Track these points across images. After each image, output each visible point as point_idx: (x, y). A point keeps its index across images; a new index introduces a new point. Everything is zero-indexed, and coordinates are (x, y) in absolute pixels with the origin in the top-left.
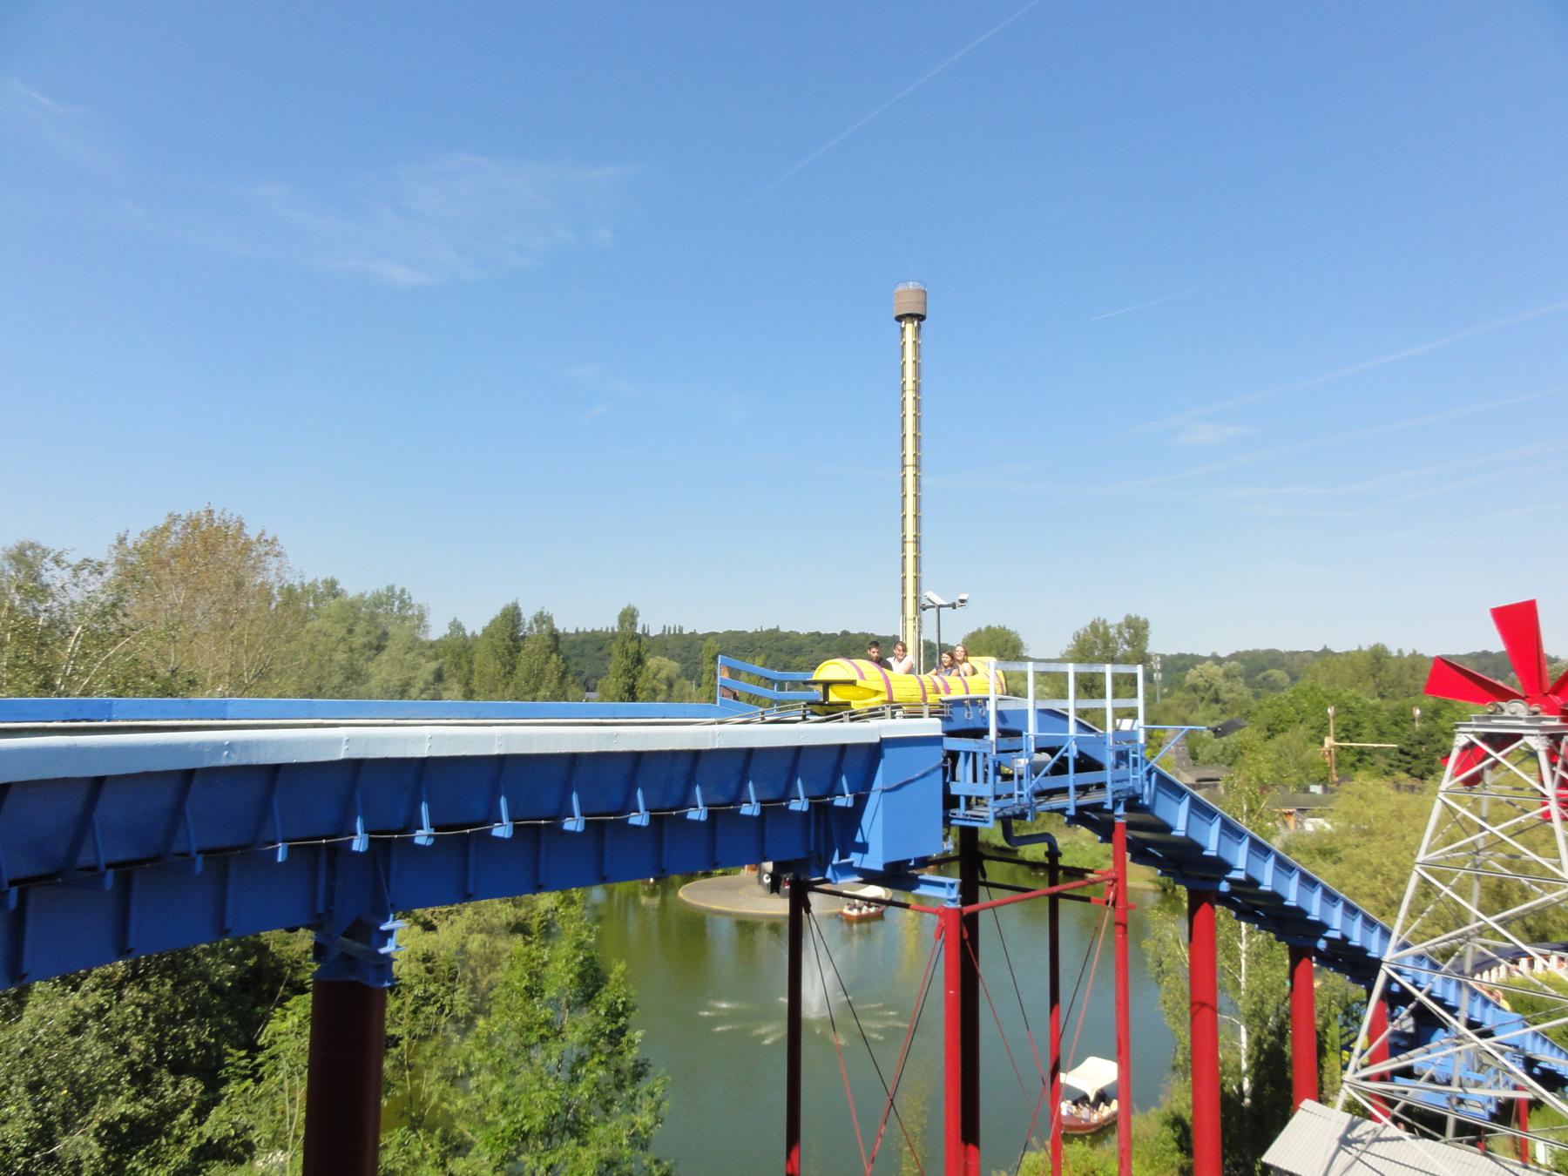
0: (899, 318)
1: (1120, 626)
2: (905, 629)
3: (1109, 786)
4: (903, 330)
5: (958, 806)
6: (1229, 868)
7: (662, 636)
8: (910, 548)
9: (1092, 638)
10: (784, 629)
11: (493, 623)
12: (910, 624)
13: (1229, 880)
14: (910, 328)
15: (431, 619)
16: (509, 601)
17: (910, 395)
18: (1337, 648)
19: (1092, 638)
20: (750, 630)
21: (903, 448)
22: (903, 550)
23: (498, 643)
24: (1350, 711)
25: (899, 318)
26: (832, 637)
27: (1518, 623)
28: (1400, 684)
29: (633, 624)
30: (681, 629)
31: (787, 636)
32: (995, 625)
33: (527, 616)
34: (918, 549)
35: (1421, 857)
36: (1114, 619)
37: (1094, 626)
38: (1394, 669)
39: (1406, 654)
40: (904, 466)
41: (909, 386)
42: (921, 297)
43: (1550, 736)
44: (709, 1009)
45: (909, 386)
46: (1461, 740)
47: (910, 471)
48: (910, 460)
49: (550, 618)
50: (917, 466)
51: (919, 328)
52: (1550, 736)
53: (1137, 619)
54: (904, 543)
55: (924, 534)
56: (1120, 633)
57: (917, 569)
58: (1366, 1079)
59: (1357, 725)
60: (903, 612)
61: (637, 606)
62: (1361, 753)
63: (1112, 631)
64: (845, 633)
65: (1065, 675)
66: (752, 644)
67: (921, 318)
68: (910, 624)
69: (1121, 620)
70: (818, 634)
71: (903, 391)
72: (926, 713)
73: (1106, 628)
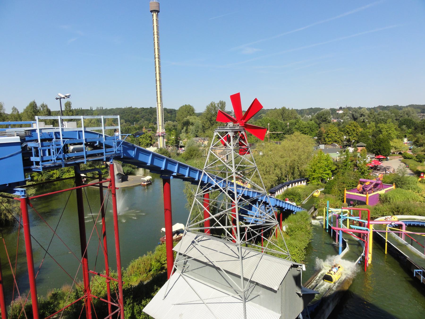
0: (151, 11)
1: (218, 104)
2: (158, 106)
3: (104, 154)
4: (153, 15)
5: (33, 165)
6: (173, 172)
7: (97, 110)
8: (158, 82)
9: (211, 107)
10: (133, 107)
11: (27, 108)
12: (159, 105)
13: (173, 176)
14: (155, 15)
15: (5, 107)
16: (31, 101)
17: (156, 36)
18: (298, 109)
19: (211, 107)
20: (123, 108)
21: (155, 53)
22: (156, 83)
23: (29, 114)
24: (275, 124)
25: (151, 11)
26: (147, 109)
27: (236, 99)
28: (289, 117)
29: (70, 107)
30: (102, 108)
31: (134, 109)
32: (187, 104)
33: (39, 105)
34: (160, 83)
35: (205, 168)
36: (217, 102)
37: (211, 104)
38: (287, 113)
39: (290, 109)
40: (155, 58)
41: (156, 33)
42: (158, 4)
43: (235, 132)
44: (88, 216)
45: (156, 33)
46: (215, 134)
47: (157, 60)
48: (157, 56)
49: (46, 106)
50: (159, 58)
51: (157, 16)
52: (235, 132)
53: (223, 101)
54: (156, 81)
55: (162, 78)
56: (218, 105)
57: (160, 89)
58: (190, 228)
59: (277, 127)
60: (157, 101)
61: (71, 101)
62: (277, 134)
63: (216, 105)
64: (151, 108)
65: (101, 119)
66: (124, 112)
67: (158, 12)
68: (159, 105)
69: (218, 102)
70: (143, 108)
71: (154, 35)
72: (16, 135)
73: (215, 105)
